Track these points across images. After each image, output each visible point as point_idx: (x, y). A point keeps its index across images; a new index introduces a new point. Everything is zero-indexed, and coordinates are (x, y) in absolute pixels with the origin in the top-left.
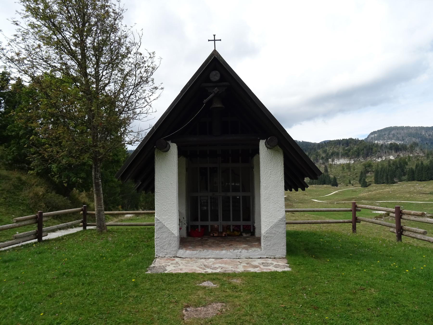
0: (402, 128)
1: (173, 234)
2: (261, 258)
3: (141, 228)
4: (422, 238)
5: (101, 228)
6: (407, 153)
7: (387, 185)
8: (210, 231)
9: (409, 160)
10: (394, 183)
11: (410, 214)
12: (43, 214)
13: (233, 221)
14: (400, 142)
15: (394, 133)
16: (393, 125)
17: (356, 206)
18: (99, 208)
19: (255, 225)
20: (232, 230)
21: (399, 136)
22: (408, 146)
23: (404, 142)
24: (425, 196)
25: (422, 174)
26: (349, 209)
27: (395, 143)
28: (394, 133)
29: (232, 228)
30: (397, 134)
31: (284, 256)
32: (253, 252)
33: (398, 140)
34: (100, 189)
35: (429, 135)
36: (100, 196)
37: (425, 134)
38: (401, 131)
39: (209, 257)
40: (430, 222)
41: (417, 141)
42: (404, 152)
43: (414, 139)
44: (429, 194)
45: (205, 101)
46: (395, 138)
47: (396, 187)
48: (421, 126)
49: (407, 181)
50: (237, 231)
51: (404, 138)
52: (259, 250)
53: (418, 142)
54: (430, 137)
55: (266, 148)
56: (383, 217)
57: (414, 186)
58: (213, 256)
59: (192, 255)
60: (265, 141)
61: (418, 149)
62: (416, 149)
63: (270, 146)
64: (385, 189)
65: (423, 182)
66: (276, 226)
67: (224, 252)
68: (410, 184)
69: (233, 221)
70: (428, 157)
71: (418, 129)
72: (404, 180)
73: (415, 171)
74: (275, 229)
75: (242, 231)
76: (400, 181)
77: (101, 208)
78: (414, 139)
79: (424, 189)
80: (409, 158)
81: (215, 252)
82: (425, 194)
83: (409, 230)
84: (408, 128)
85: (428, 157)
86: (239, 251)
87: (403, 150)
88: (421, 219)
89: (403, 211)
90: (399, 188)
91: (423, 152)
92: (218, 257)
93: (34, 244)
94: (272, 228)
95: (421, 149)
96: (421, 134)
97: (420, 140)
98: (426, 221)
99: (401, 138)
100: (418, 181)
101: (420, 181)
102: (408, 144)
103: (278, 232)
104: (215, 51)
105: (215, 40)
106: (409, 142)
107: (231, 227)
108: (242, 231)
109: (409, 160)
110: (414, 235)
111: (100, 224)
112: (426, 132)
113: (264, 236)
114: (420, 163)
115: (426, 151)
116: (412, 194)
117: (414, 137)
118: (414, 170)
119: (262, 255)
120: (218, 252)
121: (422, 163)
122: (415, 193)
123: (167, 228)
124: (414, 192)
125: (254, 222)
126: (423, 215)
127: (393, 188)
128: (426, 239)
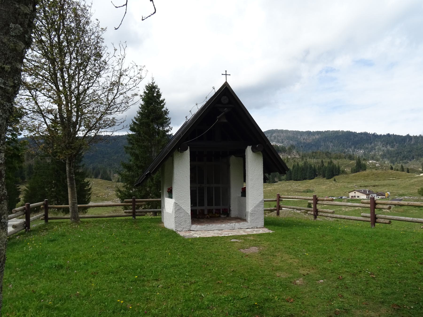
0: (282, 131)
1: (188, 213)
2: (248, 228)
3: (99, 220)
4: (332, 216)
5: (76, 219)
6: (286, 155)
7: (269, 184)
8: (198, 213)
9: (288, 161)
10: (275, 182)
11: (323, 200)
12: (31, 205)
13: (215, 205)
14: (280, 144)
15: (275, 136)
16: (274, 128)
17: (280, 197)
18: (73, 200)
19: (231, 208)
20: (214, 213)
21: (280, 138)
22: (287, 148)
23: (283, 144)
24: (300, 194)
25: (298, 174)
26: (275, 199)
27: (276, 145)
28: (275, 136)
29: (214, 211)
30: (278, 136)
31: (263, 226)
32: (242, 224)
33: (278, 143)
34: (74, 183)
35: (304, 139)
36: (74, 190)
37: (301, 138)
38: (281, 134)
39: (214, 229)
40: (338, 204)
41: (294, 143)
42: (284, 154)
43: (291, 142)
44: (302, 192)
45: (218, 117)
46: (276, 140)
47: (276, 186)
48: (297, 130)
49: (285, 181)
50: (218, 213)
51: (283, 141)
52: (247, 223)
53: (294, 144)
54: (304, 141)
55: (252, 152)
56: (267, 214)
57: (291, 185)
58: (216, 229)
59: (202, 228)
60: (251, 147)
61: (294, 151)
62: (293, 151)
63: (254, 150)
64: (267, 188)
65: (298, 181)
66: (258, 206)
67: (224, 225)
68: (287, 183)
69: (215, 205)
70: (303, 159)
71: (295, 133)
72: (283, 180)
73: (292, 171)
74: (257, 208)
75: (221, 213)
76: (280, 181)
77: (75, 200)
78: (291, 142)
79: (299, 188)
80: (288, 160)
81: (217, 225)
82: (300, 192)
83: (322, 212)
84: (287, 131)
85: (303, 159)
86: (234, 224)
87: (283, 152)
88: (331, 203)
89: (319, 198)
90: (279, 187)
91: (299, 154)
92: (220, 229)
93: (86, 222)
94: (255, 207)
95: (297, 152)
96: (297, 138)
97: (296, 143)
98: (335, 204)
99: (281, 141)
100: (294, 180)
101: (296, 180)
102: (286, 146)
103: (259, 210)
104: (226, 82)
105: (226, 75)
106: (287, 145)
107: (214, 210)
108: (221, 213)
109: (288, 161)
110: (326, 214)
111: (75, 215)
112: (302, 135)
113: (250, 213)
114: (296, 164)
115: (301, 153)
116: (290, 193)
117: (291, 140)
118: (292, 170)
119: (248, 226)
120: (219, 225)
121: (298, 164)
122: (291, 191)
123: (183, 209)
124: (291, 191)
125: (230, 206)
126: (332, 200)
127: (274, 186)
128: (335, 216)
